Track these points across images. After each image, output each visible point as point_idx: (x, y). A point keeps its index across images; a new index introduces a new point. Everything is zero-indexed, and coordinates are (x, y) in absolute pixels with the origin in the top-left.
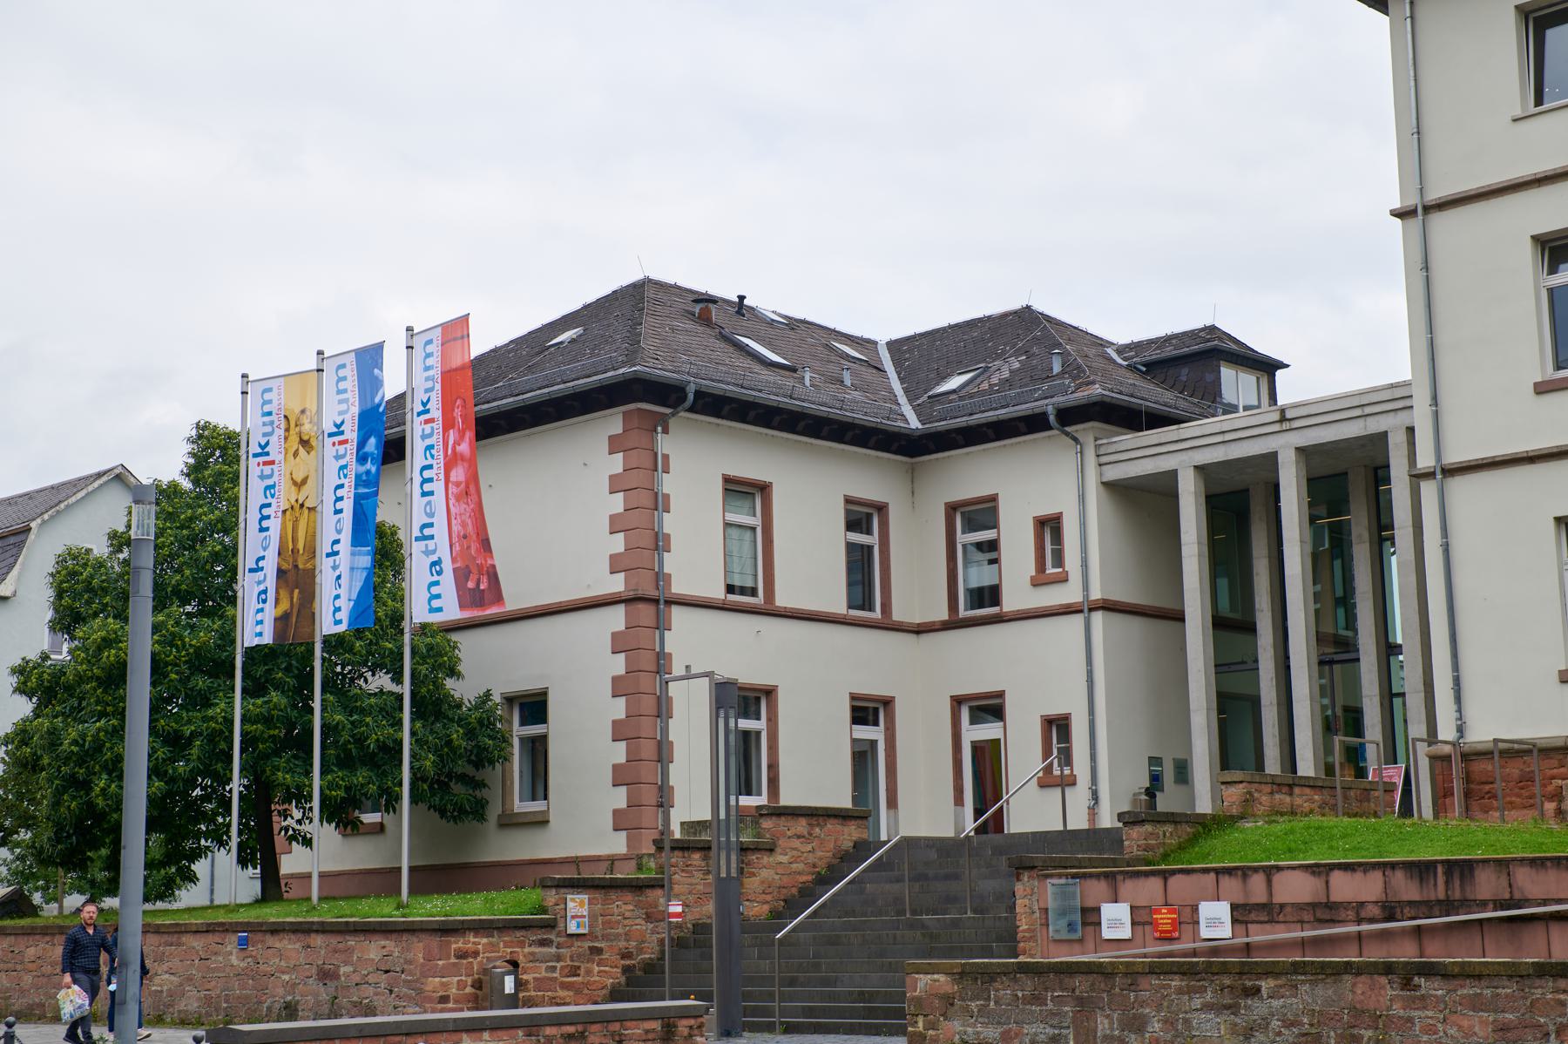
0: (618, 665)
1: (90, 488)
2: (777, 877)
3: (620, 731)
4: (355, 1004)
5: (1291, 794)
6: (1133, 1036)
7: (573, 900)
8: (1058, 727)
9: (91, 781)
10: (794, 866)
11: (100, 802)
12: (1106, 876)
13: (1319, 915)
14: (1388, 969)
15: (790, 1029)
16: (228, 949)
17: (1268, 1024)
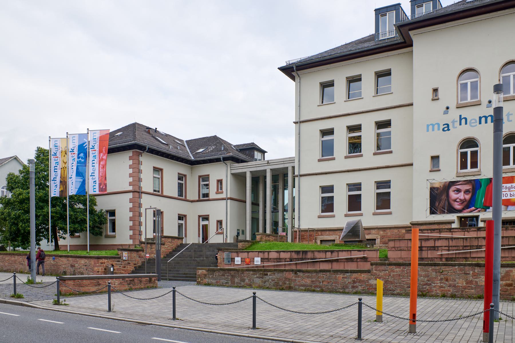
0: (131, 205)
1: (9, 160)
2: (165, 250)
3: (131, 219)
4: (79, 272)
5: (269, 237)
6: (242, 283)
7: (124, 253)
8: (220, 222)
9: (18, 224)
10: (168, 248)
11: (21, 228)
12: (236, 252)
13: (278, 260)
14: (292, 271)
15: (170, 280)
16: (51, 260)
17: (269, 280)
